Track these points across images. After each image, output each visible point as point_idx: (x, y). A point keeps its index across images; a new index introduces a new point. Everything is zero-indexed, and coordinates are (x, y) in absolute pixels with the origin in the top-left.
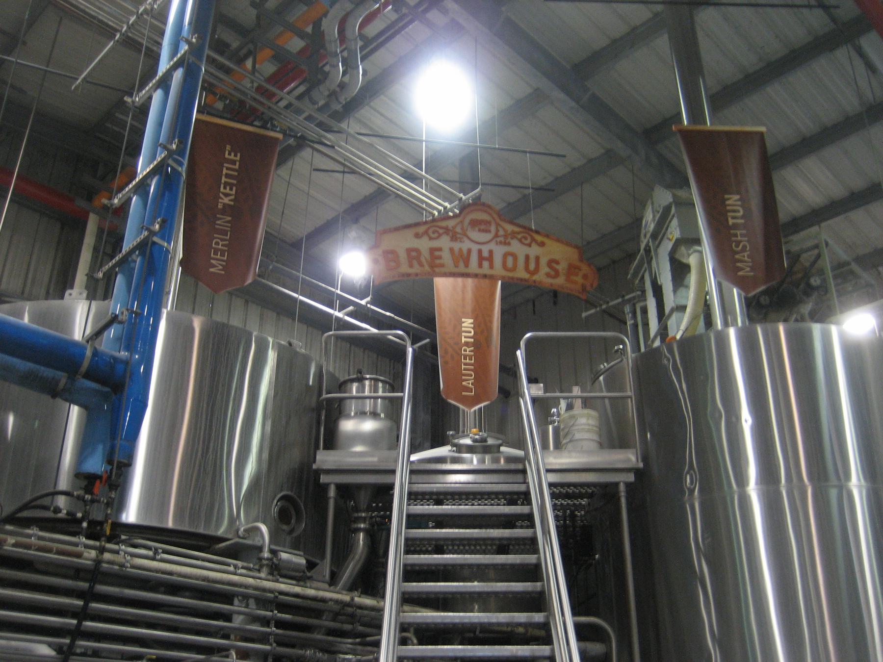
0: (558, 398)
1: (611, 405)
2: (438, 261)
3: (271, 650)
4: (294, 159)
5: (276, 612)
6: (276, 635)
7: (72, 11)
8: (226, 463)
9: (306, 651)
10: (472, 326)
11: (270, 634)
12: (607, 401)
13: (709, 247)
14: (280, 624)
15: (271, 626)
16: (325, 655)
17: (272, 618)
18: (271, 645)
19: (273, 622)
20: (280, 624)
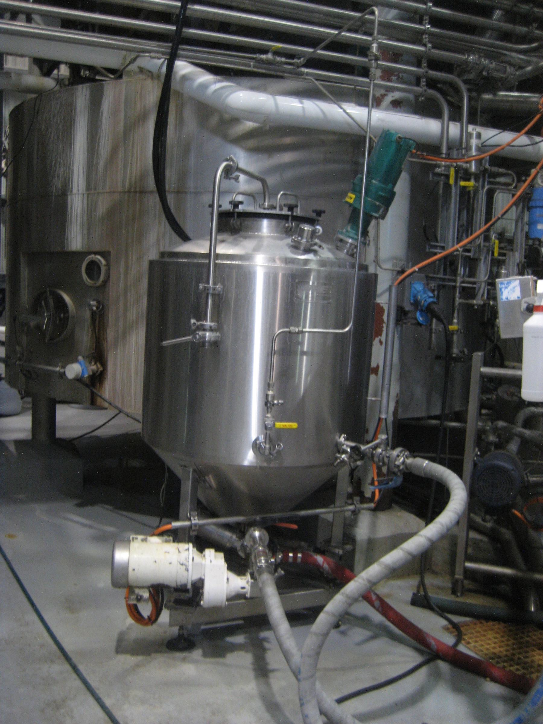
0: (216, 265)
1: (203, 264)
2: (326, 290)
3: (426, 52)
4: (501, 132)
5: (430, 4)
6: (431, 34)
7: (489, 261)
8: (147, 18)
9: (469, 56)
10: (169, 51)
11: (423, 32)
12: (207, 261)
13: (92, 14)
14: (436, 21)
15: (424, 22)
16: (492, 63)
17: (426, 12)
18: (425, 45)
19: (427, 18)
20: (436, 21)
